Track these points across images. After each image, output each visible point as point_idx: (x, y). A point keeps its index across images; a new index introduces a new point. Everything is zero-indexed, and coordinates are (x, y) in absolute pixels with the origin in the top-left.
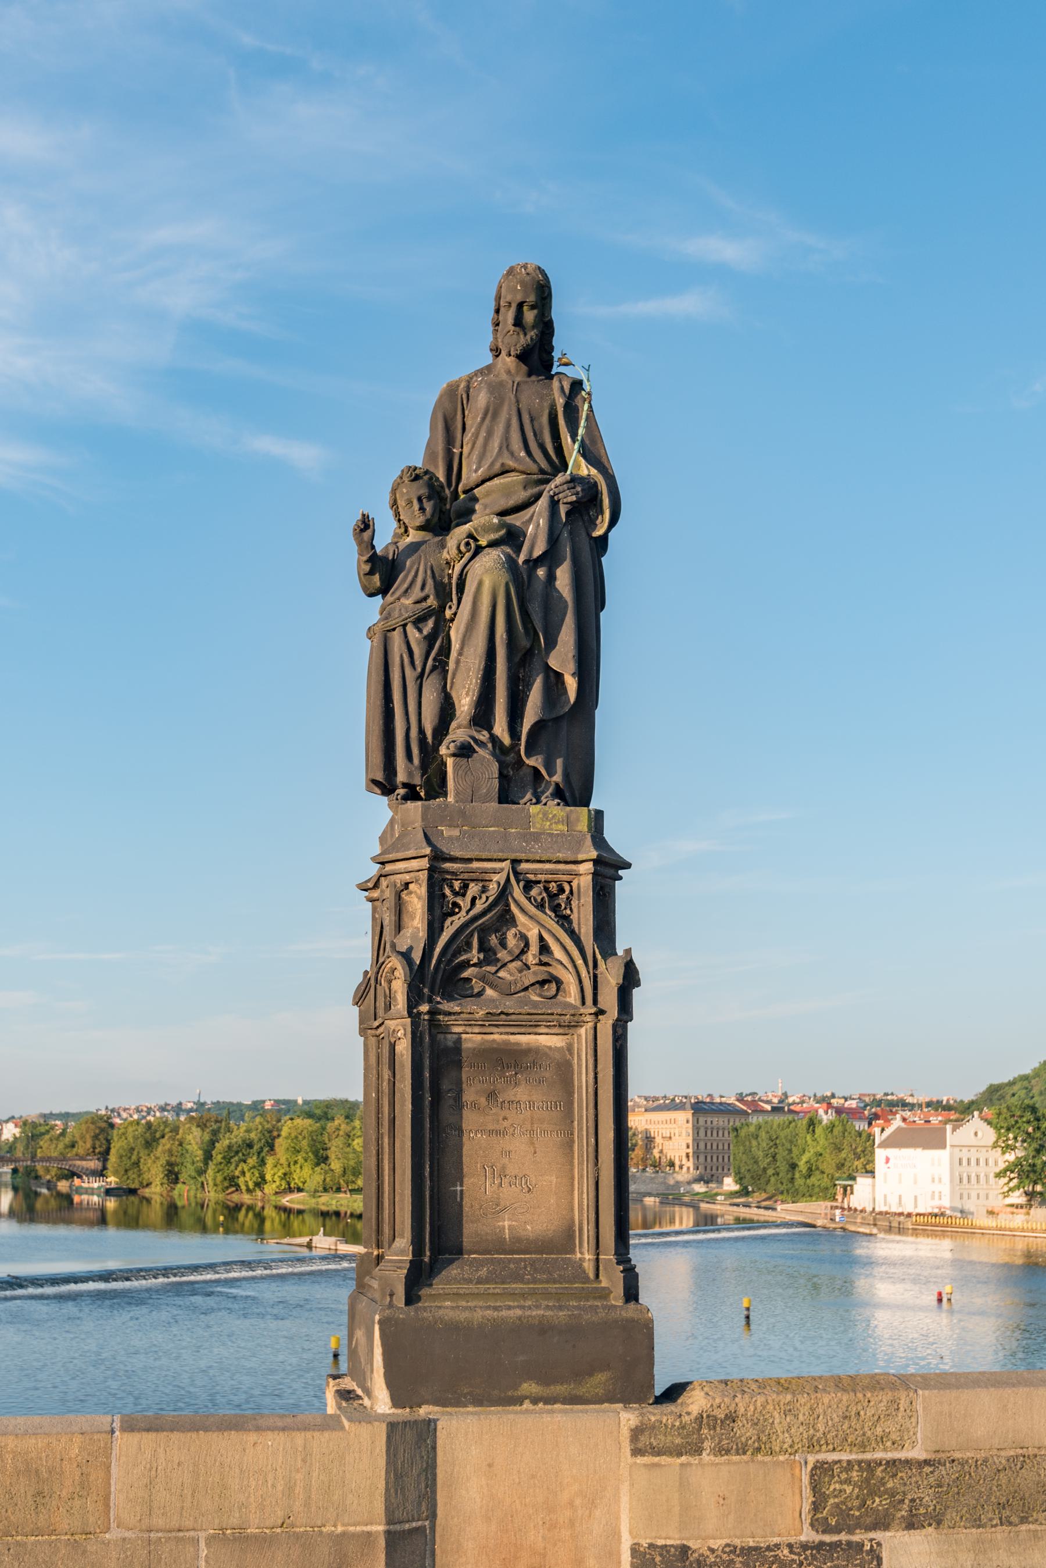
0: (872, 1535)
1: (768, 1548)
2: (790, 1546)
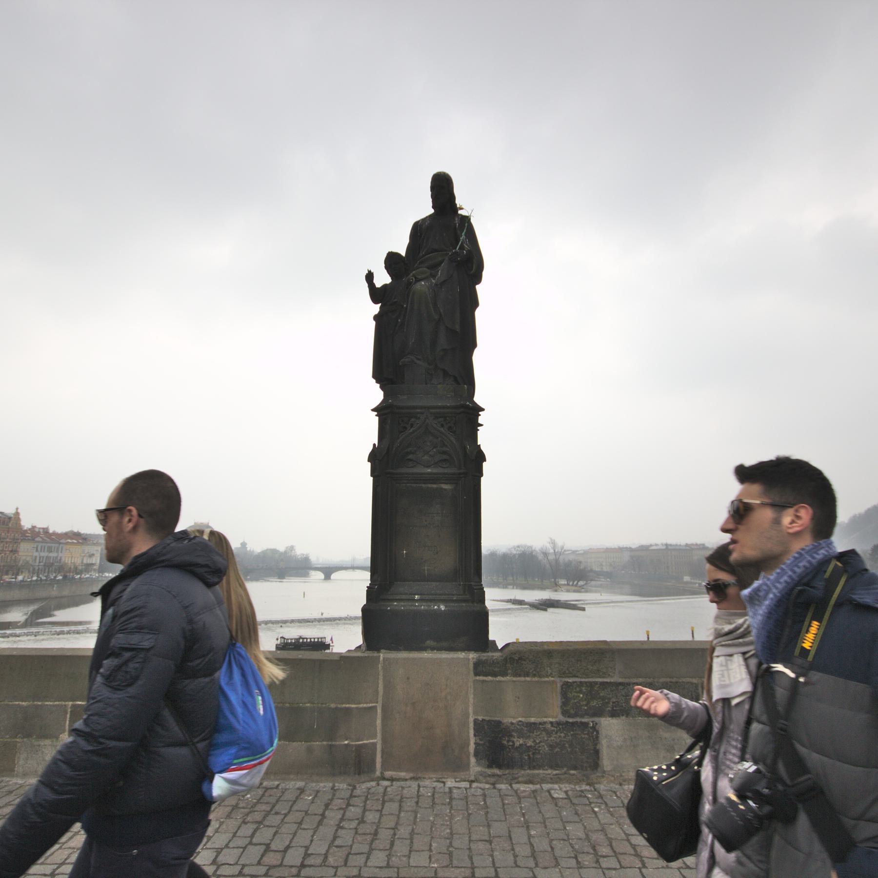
0: (593, 719)
1: (540, 724)
2: (551, 723)
